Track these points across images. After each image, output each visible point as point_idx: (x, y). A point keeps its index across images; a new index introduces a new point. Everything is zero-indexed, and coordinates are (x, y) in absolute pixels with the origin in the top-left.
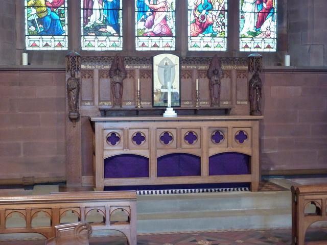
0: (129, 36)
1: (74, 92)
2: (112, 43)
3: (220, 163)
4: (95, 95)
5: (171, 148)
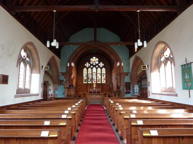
0: (92, 82)
1: (87, 87)
2: (91, 83)
3: (98, 92)
4: (89, 87)
5: (94, 91)
